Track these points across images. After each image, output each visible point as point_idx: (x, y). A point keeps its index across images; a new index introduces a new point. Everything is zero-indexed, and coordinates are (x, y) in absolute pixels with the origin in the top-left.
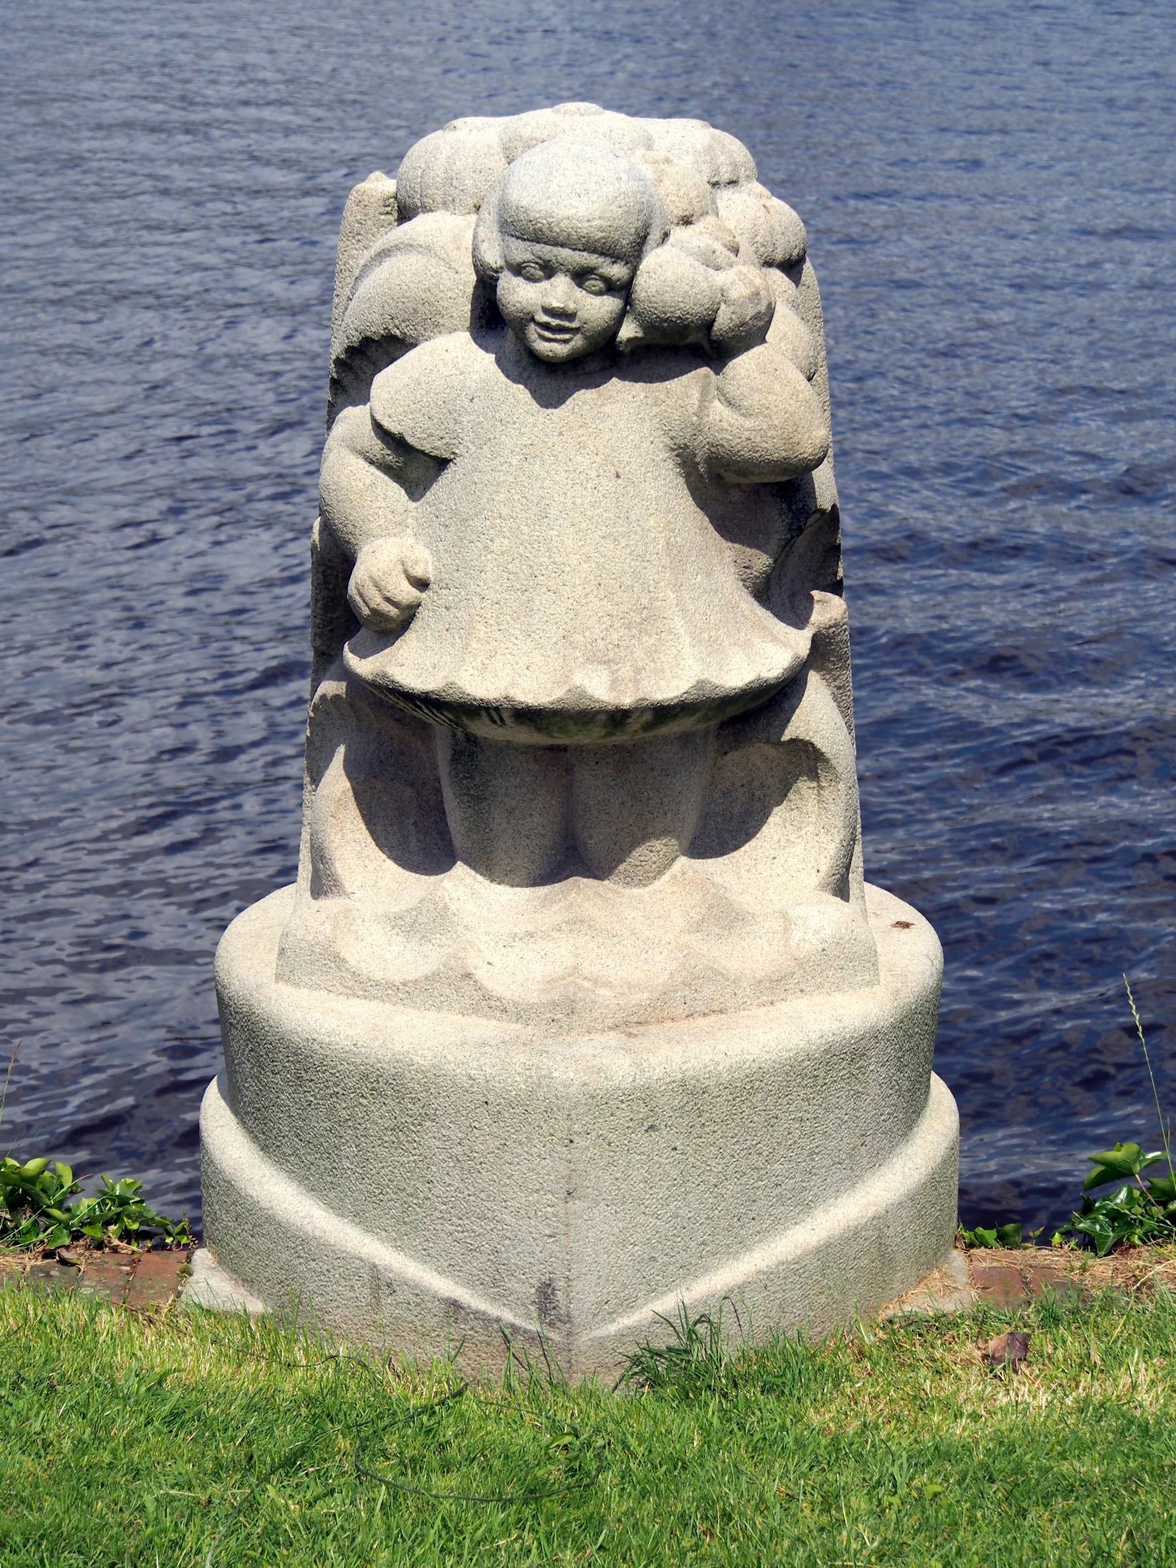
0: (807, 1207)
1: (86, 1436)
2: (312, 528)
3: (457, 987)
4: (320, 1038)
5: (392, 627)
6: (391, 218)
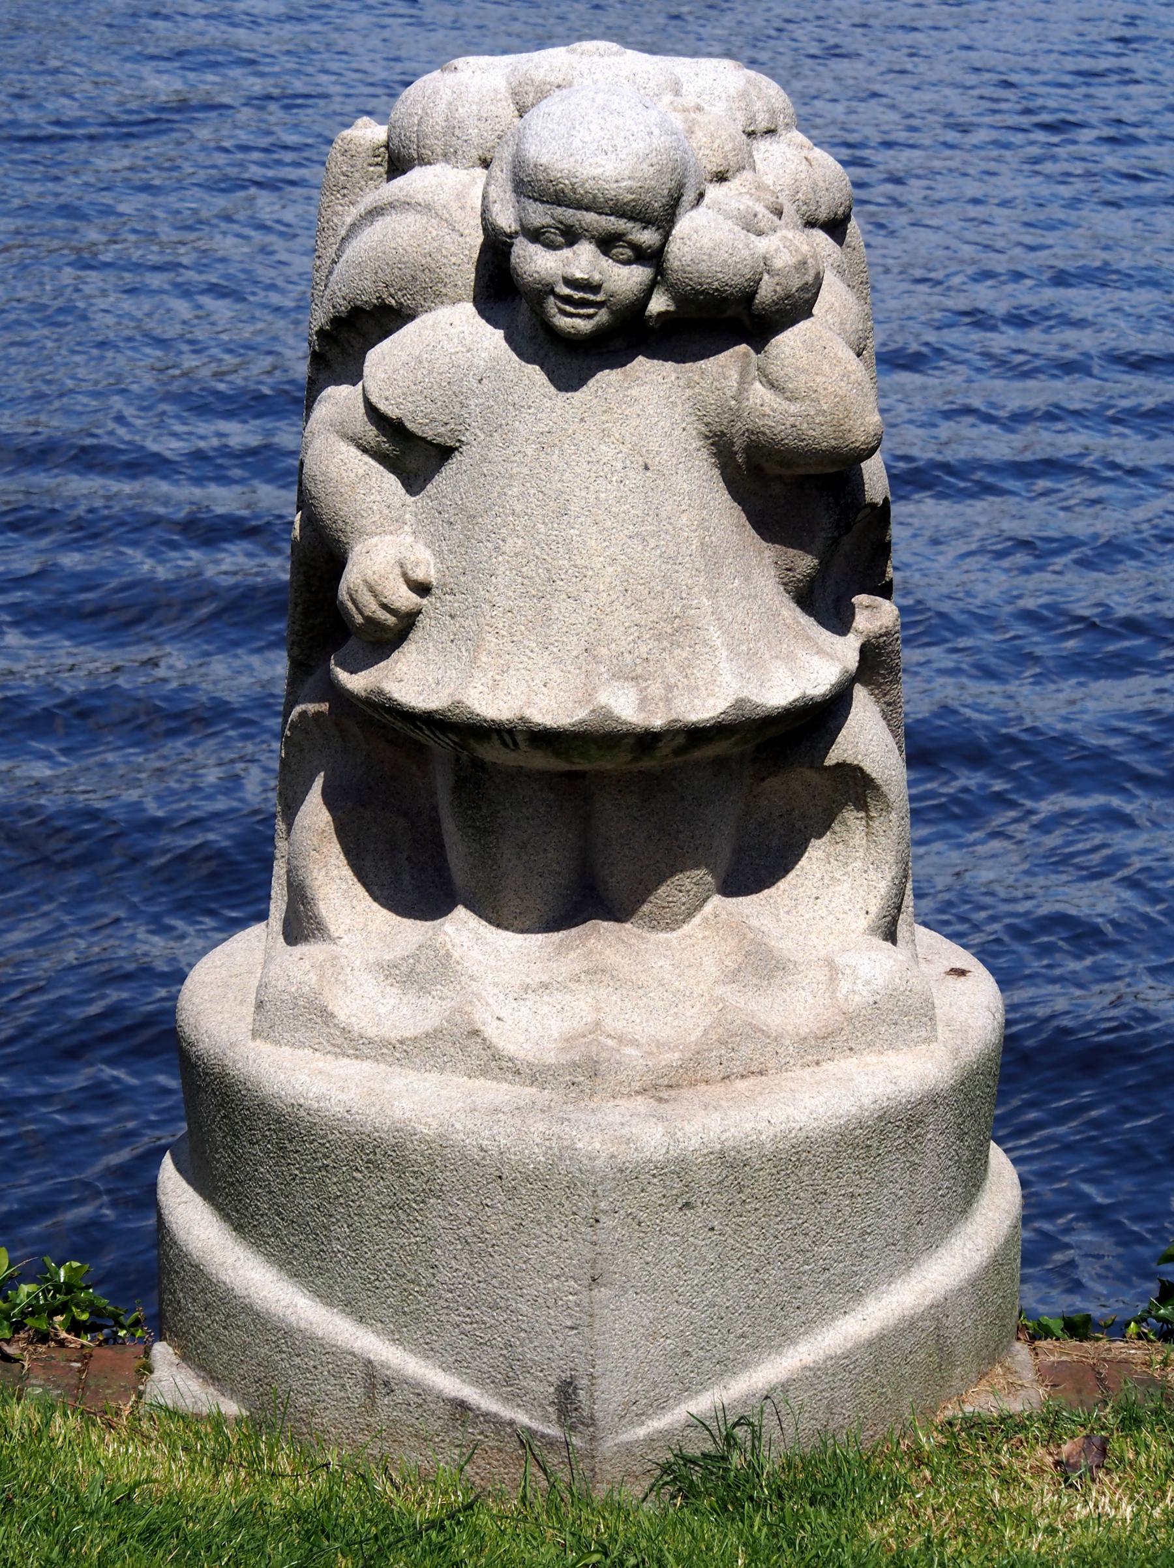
0: (858, 1295)
1: (54, 1555)
2: (292, 523)
3: (461, 1045)
4: (307, 1104)
5: (387, 637)
6: (381, 169)
